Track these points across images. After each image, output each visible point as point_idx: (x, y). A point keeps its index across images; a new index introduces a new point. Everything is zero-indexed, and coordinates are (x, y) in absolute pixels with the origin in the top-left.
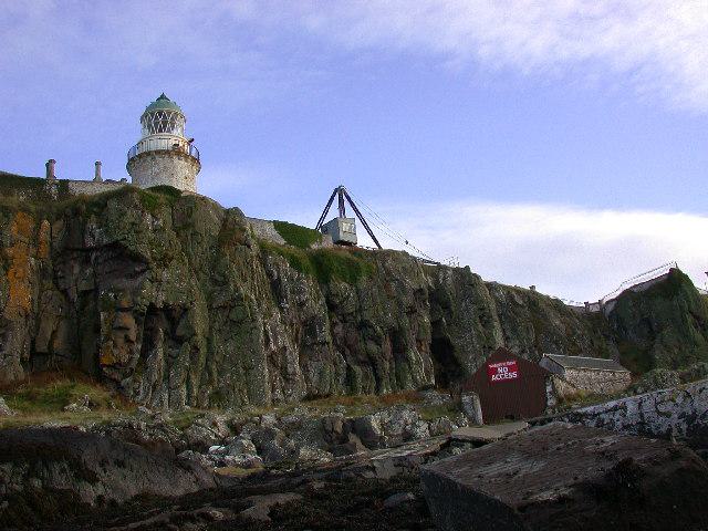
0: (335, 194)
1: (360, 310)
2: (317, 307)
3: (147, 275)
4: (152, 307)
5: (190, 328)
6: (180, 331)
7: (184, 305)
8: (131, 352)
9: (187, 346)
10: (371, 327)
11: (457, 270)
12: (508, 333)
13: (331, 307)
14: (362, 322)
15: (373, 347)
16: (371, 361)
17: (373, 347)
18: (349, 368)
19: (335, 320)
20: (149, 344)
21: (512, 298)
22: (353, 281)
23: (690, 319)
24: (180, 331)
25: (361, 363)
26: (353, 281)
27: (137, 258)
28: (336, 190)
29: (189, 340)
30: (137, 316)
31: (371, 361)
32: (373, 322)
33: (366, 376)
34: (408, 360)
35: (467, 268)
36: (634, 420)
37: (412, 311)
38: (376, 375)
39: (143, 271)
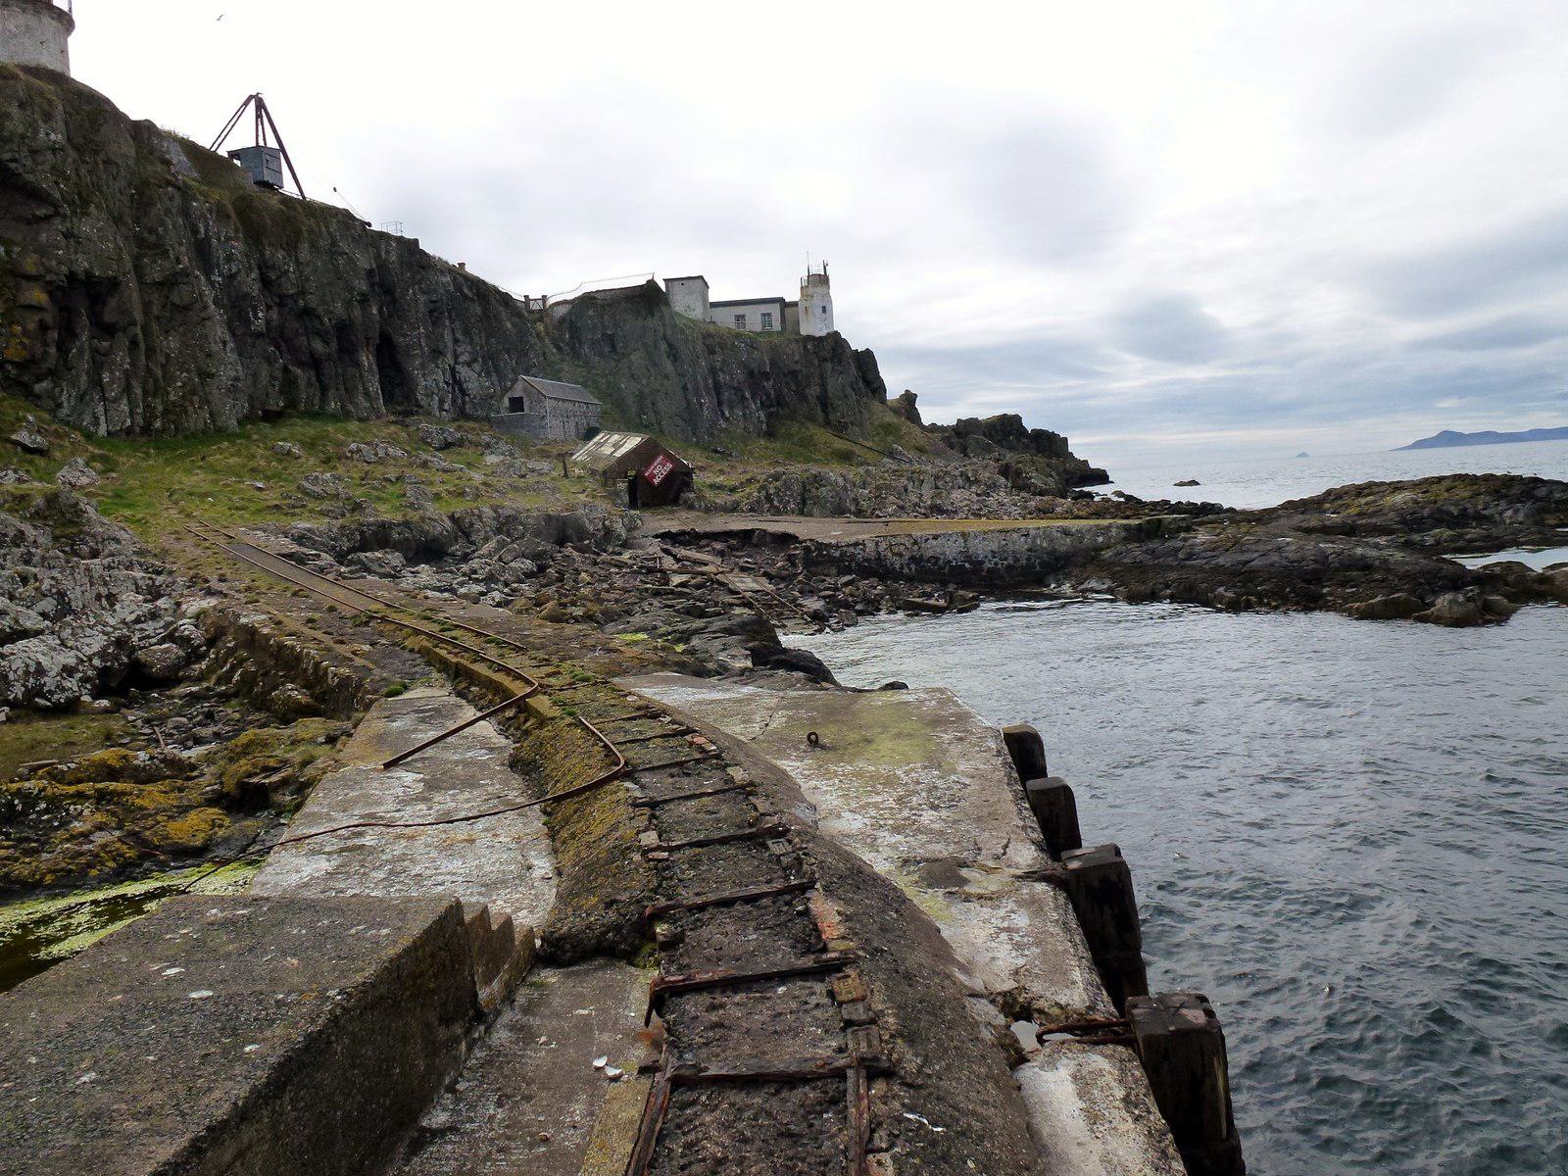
0: (246, 103)
1: (302, 293)
2: (250, 283)
3: (58, 224)
4: (72, 277)
5: (125, 312)
6: (109, 316)
7: (115, 278)
8: (45, 344)
9: (123, 341)
10: (319, 317)
11: (400, 240)
12: (459, 336)
13: (266, 282)
14: (306, 306)
15: (318, 346)
16: (315, 363)
17: (318, 346)
18: (286, 370)
19: (270, 302)
20: (68, 331)
21: (459, 288)
22: (292, 247)
23: (664, 346)
24: (109, 316)
25: (301, 364)
26: (292, 247)
27: (35, 195)
28: (251, 98)
29: (124, 330)
30: (51, 289)
31: (315, 363)
32: (320, 310)
33: (309, 384)
34: (358, 365)
35: (462, 265)
36: (873, 555)
37: (364, 300)
38: (319, 381)
39: (47, 218)
